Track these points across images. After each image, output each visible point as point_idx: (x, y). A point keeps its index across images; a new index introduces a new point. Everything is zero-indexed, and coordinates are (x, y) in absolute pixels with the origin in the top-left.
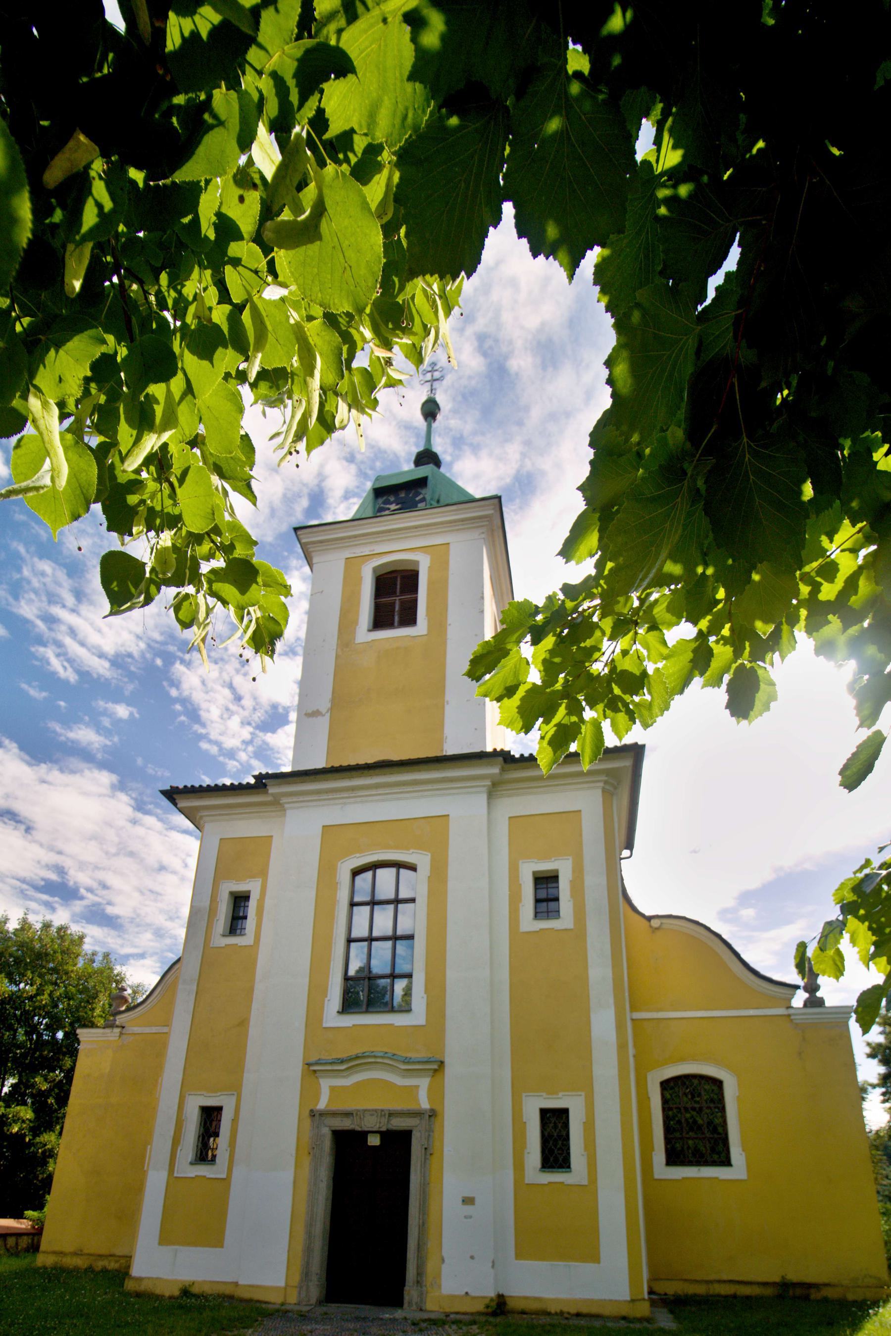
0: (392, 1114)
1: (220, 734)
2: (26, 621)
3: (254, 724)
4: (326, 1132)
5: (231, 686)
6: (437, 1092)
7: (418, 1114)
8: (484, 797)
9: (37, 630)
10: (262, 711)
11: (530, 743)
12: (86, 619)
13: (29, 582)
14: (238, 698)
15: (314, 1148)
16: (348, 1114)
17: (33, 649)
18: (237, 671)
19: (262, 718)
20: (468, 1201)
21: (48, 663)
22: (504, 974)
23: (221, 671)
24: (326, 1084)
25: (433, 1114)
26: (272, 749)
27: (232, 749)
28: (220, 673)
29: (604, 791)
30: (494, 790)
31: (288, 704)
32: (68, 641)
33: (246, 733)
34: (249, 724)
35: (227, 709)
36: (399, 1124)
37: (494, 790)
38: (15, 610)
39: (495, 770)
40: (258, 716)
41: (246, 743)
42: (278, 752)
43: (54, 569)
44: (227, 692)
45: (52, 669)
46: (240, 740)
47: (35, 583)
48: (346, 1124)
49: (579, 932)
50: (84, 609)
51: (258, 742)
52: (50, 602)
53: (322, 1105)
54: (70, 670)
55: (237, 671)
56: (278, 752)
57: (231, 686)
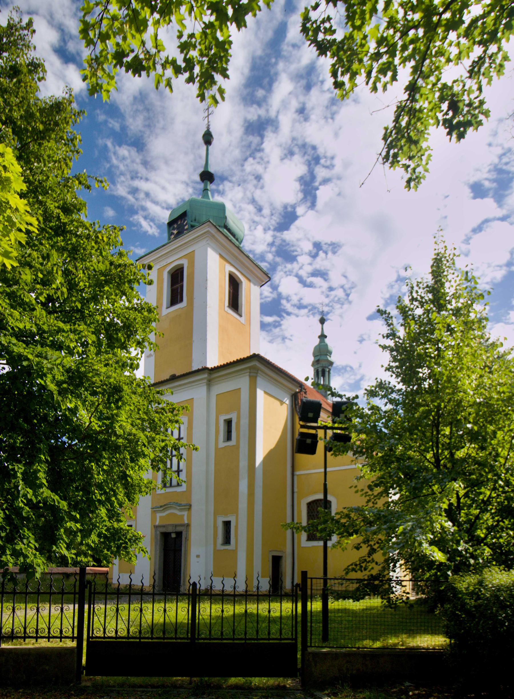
0: (176, 526)
1: (252, 244)
2: (122, 198)
3: (272, 228)
4: (158, 533)
5: (253, 201)
6: (189, 517)
7: (183, 525)
8: (205, 388)
9: (129, 203)
10: (277, 215)
11: (504, 167)
12: (156, 183)
13: (118, 167)
14: (260, 209)
15: (156, 538)
16: (164, 526)
17: (131, 219)
18: (256, 187)
19: (278, 221)
20: (198, 556)
21: (141, 226)
22: (212, 467)
23: (245, 190)
24: (158, 515)
25: (188, 525)
26: (288, 244)
27: (262, 252)
28: (245, 193)
29: (250, 376)
30: (210, 383)
31: (294, 202)
32: (149, 205)
33: (269, 237)
34: (269, 229)
35: (254, 222)
36: (179, 529)
37: (210, 383)
38: (115, 193)
39: (206, 376)
40: (275, 220)
41: (272, 244)
42: (293, 246)
43: (129, 151)
44: (251, 208)
45: (143, 229)
46: (266, 244)
47: (122, 167)
48: (164, 530)
49: (237, 447)
50: (152, 175)
51: (278, 242)
52: (132, 178)
53: (157, 523)
54: (154, 226)
55: (256, 187)
56: (293, 246)
57: (253, 201)
